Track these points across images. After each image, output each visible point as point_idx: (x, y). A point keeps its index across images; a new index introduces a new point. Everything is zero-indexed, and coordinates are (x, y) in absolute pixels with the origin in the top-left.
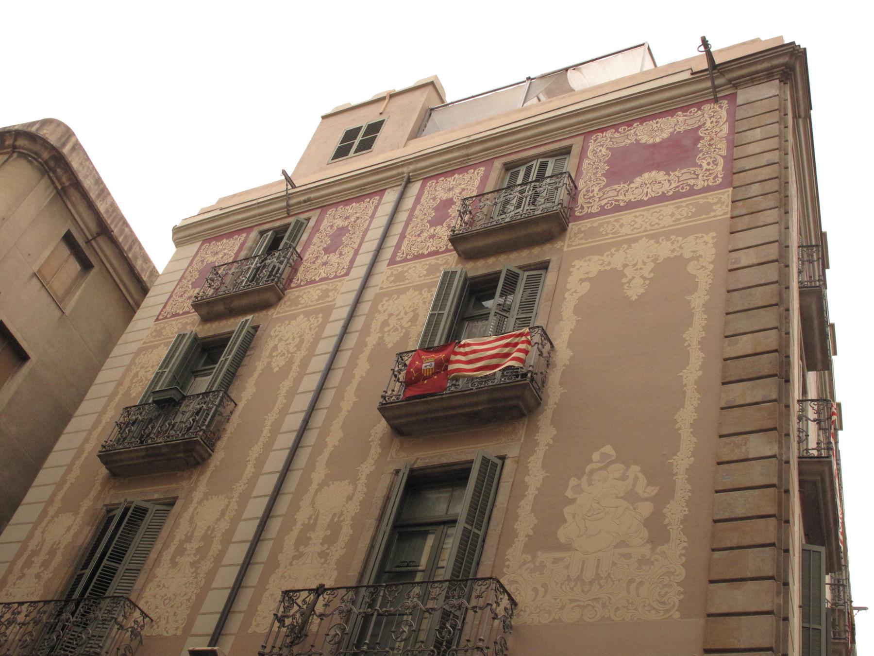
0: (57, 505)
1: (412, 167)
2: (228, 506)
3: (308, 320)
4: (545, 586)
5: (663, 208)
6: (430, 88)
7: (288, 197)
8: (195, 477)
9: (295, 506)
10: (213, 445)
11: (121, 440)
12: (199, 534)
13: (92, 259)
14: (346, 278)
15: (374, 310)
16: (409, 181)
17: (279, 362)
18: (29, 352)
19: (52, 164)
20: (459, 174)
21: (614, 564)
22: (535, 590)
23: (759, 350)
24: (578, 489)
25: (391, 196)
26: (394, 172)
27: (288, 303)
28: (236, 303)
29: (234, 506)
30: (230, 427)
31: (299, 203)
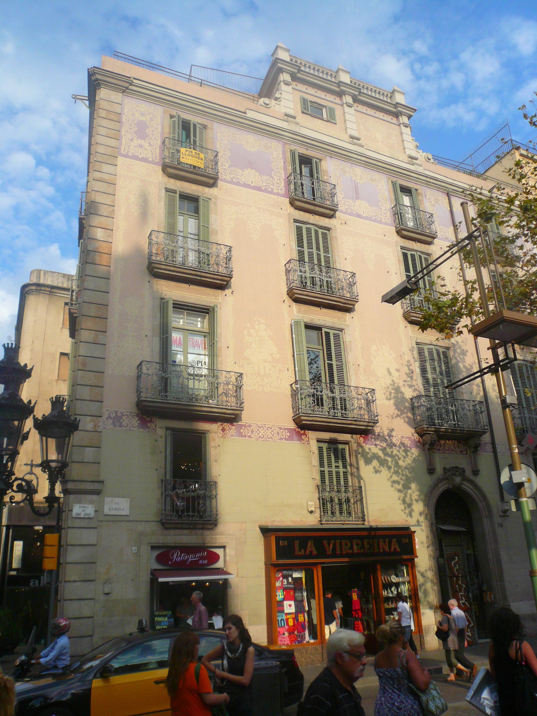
19: (38, 288)
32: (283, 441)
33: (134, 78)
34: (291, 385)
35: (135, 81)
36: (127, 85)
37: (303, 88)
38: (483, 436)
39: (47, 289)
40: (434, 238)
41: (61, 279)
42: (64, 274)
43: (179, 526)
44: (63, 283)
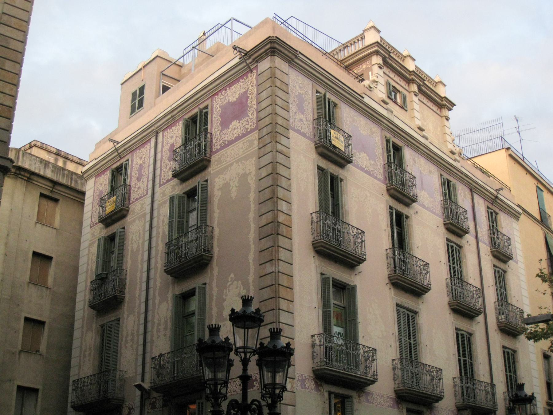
0: (85, 328)
1: (156, 126)
6: (158, 58)
7: (116, 150)
9: (153, 316)
10: (124, 293)
11: (94, 298)
12: (130, 333)
13: (57, 197)
16: (157, 133)
17: (135, 246)
18: (42, 319)
19: (18, 172)
23: (268, 222)
25: (153, 140)
26: (150, 130)
27: (132, 213)
28: (113, 218)
29: (137, 319)
30: (128, 282)
31: (122, 152)
33: (300, 53)
34: (454, 378)
35: (300, 55)
36: (293, 57)
37: (392, 75)
38: (371, 386)
39: (26, 174)
40: (414, 201)
41: (38, 164)
42: (42, 159)
44: (40, 170)
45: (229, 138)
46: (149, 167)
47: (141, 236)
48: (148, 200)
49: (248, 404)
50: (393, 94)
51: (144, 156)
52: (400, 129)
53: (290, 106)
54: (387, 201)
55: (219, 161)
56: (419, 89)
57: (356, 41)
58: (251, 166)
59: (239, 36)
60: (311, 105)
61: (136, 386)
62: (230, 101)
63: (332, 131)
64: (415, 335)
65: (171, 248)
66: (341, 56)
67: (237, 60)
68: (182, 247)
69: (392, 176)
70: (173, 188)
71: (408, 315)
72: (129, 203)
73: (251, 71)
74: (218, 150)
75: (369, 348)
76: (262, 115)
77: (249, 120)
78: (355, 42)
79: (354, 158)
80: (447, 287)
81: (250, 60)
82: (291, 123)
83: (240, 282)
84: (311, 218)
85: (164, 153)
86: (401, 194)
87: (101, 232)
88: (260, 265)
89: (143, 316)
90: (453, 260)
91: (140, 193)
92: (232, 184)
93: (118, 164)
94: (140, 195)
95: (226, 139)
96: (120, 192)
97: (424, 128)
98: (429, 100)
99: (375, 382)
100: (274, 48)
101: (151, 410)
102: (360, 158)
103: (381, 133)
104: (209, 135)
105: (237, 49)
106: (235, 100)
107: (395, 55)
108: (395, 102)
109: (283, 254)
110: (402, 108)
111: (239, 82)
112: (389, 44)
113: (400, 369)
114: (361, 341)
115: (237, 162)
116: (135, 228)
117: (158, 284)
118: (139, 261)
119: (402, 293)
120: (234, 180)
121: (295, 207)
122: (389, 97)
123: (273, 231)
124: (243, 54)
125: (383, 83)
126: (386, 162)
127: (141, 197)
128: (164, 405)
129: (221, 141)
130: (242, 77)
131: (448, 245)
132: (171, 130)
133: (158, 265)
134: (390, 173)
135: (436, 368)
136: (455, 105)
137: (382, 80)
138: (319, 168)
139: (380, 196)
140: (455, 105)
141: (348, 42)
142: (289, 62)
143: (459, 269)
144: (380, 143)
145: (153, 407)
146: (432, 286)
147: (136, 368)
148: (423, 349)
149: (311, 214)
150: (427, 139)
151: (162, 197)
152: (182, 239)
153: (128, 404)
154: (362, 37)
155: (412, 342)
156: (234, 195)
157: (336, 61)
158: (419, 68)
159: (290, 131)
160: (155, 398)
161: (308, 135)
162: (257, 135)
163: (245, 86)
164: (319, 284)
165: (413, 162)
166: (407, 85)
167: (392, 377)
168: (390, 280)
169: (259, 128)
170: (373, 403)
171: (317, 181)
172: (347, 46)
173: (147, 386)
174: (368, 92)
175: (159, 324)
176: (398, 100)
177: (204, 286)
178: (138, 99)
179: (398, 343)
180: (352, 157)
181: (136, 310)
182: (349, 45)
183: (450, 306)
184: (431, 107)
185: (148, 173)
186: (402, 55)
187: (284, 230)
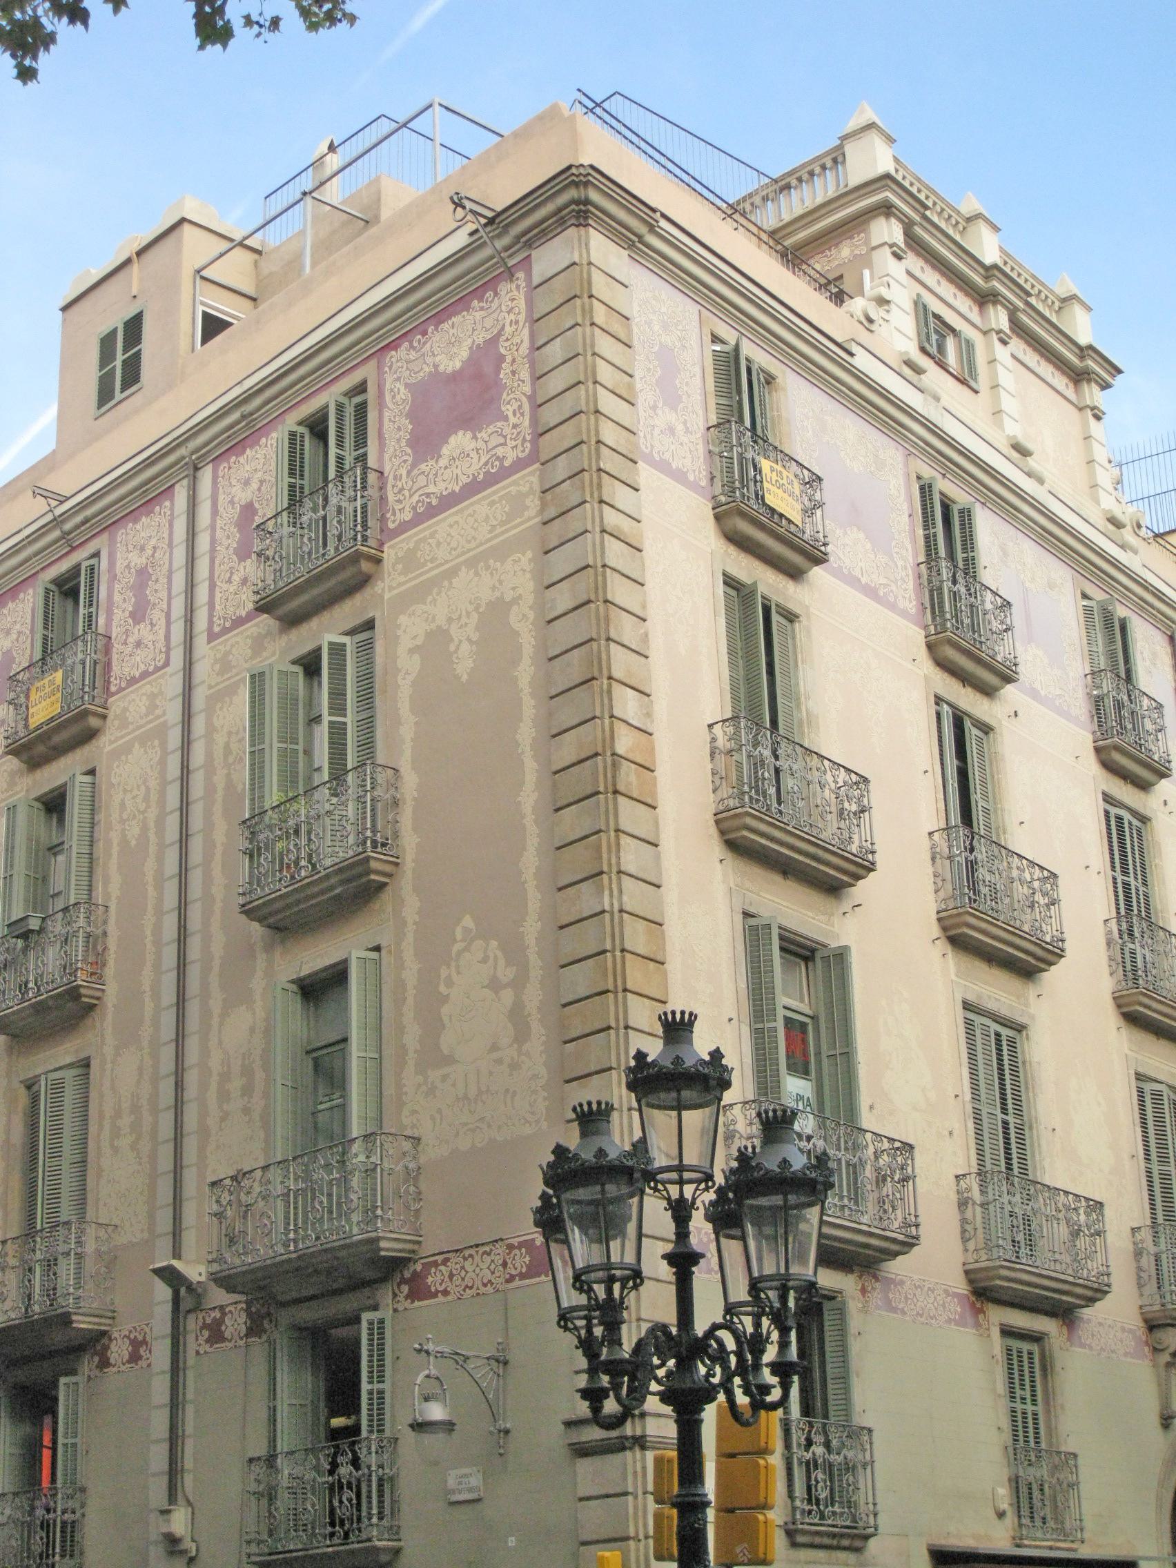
1: (192, 445)
2: (142, 1061)
3: (146, 752)
4: (439, 1111)
5: (477, 507)
7: (57, 522)
8: (98, 1025)
9: (205, 1052)
12: (125, 1105)
14: (167, 669)
15: (211, 729)
17: (134, 831)
20: (251, 447)
21: (491, 1073)
22: (432, 1118)
23: (583, 756)
24: (449, 983)
26: (171, 459)
28: (57, 739)
31: (77, 527)
32: (517, 1283)
33: (663, 216)
35: (663, 223)
36: (642, 229)
37: (931, 277)
40: (1008, 679)
43: (845, 1542)
45: (439, 488)
46: (170, 578)
47: (154, 797)
48: (172, 683)
49: (697, 1339)
50: (934, 337)
51: (153, 542)
52: (961, 453)
53: (639, 386)
54: (926, 678)
55: (409, 561)
56: (1015, 324)
57: (817, 170)
58: (517, 576)
59: (459, 162)
60: (698, 381)
61: (157, 1272)
62: (441, 368)
63: (765, 465)
64: (1017, 1099)
65: (261, 837)
66: (769, 218)
67: (461, 239)
68: (297, 832)
69: (941, 603)
70: (258, 645)
71: (998, 1035)
72: (108, 693)
73: (510, 273)
74: (404, 527)
75: (891, 1140)
76: (551, 415)
77: (507, 431)
78: (812, 174)
79: (829, 549)
80: (1108, 944)
81: (506, 240)
82: (642, 441)
83: (494, 943)
84: (709, 740)
85: (219, 534)
86: (967, 654)
87: (12, 784)
88: (560, 889)
89: (168, 1053)
90: (1124, 863)
91: (140, 661)
92: (454, 630)
93: (64, 566)
94: (142, 667)
95: (431, 489)
96: (78, 654)
97: (1030, 446)
98: (1042, 355)
99: (914, 1245)
100: (587, 202)
101: (207, 1348)
102: (846, 546)
103: (907, 464)
104: (372, 478)
105: (468, 205)
106: (458, 365)
107: (940, 214)
108: (942, 365)
109: (632, 856)
110: (963, 382)
111: (468, 308)
112: (919, 180)
113: (982, 1205)
114: (867, 1120)
115: (472, 563)
116: (128, 771)
117: (217, 949)
118: (149, 878)
119: (980, 967)
120: (464, 620)
121: (661, 704)
122: (923, 350)
123: (593, 783)
124: (483, 221)
125: (909, 306)
126: (922, 558)
127: (145, 675)
128: (254, 1329)
129: (416, 498)
130: (479, 293)
131: (1107, 813)
132: (241, 459)
133: (214, 890)
134: (935, 594)
135: (1087, 1199)
136: (1119, 371)
137: (902, 295)
138: (730, 582)
139: (909, 665)
140: (1119, 371)
141: (790, 174)
142: (631, 246)
143: (1141, 889)
144: (903, 497)
145: (216, 1334)
146: (1067, 945)
147: (151, 1216)
148: (1043, 1143)
149: (710, 726)
150: (1041, 481)
151: (221, 673)
152: (295, 806)
153: (129, 1327)
154: (836, 158)
155: (1011, 1119)
156: (464, 665)
157: (755, 230)
158: (1008, 255)
159: (641, 464)
160: (222, 1308)
161: (691, 478)
162: (535, 479)
163: (488, 323)
164: (740, 947)
165: (1005, 557)
166: (976, 309)
167: (958, 1230)
168: (944, 929)
169: (543, 458)
170: (904, 1313)
171: (722, 621)
172: (788, 187)
173: (195, 1272)
174: (863, 336)
175: (225, 1077)
176: (952, 359)
177: (374, 955)
178: (120, 357)
179: (971, 1125)
180: (825, 545)
181: (146, 1031)
182: (794, 182)
183: (1119, 1006)
184: (1049, 379)
185: (167, 595)
186: (958, 213)
187: (633, 778)
